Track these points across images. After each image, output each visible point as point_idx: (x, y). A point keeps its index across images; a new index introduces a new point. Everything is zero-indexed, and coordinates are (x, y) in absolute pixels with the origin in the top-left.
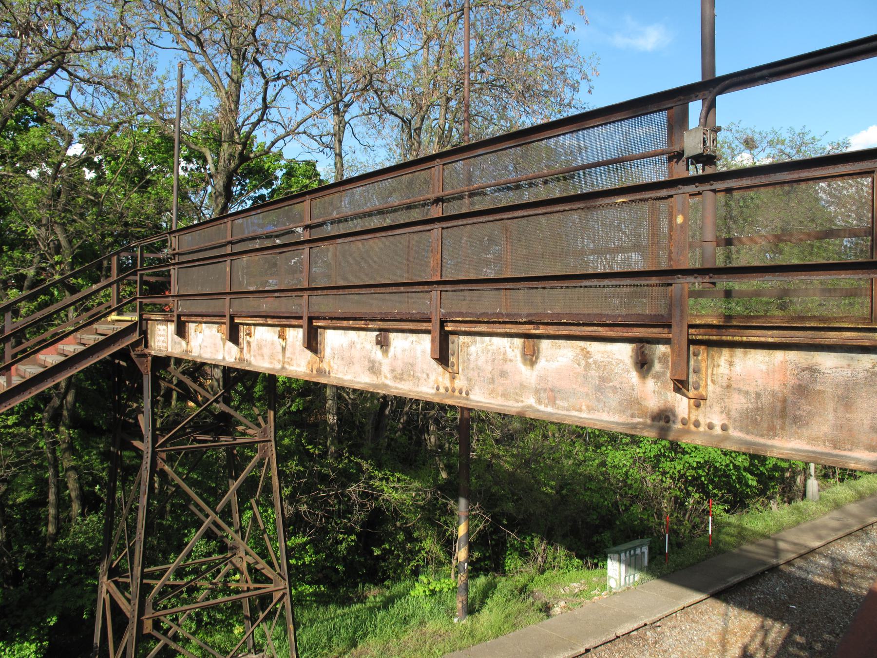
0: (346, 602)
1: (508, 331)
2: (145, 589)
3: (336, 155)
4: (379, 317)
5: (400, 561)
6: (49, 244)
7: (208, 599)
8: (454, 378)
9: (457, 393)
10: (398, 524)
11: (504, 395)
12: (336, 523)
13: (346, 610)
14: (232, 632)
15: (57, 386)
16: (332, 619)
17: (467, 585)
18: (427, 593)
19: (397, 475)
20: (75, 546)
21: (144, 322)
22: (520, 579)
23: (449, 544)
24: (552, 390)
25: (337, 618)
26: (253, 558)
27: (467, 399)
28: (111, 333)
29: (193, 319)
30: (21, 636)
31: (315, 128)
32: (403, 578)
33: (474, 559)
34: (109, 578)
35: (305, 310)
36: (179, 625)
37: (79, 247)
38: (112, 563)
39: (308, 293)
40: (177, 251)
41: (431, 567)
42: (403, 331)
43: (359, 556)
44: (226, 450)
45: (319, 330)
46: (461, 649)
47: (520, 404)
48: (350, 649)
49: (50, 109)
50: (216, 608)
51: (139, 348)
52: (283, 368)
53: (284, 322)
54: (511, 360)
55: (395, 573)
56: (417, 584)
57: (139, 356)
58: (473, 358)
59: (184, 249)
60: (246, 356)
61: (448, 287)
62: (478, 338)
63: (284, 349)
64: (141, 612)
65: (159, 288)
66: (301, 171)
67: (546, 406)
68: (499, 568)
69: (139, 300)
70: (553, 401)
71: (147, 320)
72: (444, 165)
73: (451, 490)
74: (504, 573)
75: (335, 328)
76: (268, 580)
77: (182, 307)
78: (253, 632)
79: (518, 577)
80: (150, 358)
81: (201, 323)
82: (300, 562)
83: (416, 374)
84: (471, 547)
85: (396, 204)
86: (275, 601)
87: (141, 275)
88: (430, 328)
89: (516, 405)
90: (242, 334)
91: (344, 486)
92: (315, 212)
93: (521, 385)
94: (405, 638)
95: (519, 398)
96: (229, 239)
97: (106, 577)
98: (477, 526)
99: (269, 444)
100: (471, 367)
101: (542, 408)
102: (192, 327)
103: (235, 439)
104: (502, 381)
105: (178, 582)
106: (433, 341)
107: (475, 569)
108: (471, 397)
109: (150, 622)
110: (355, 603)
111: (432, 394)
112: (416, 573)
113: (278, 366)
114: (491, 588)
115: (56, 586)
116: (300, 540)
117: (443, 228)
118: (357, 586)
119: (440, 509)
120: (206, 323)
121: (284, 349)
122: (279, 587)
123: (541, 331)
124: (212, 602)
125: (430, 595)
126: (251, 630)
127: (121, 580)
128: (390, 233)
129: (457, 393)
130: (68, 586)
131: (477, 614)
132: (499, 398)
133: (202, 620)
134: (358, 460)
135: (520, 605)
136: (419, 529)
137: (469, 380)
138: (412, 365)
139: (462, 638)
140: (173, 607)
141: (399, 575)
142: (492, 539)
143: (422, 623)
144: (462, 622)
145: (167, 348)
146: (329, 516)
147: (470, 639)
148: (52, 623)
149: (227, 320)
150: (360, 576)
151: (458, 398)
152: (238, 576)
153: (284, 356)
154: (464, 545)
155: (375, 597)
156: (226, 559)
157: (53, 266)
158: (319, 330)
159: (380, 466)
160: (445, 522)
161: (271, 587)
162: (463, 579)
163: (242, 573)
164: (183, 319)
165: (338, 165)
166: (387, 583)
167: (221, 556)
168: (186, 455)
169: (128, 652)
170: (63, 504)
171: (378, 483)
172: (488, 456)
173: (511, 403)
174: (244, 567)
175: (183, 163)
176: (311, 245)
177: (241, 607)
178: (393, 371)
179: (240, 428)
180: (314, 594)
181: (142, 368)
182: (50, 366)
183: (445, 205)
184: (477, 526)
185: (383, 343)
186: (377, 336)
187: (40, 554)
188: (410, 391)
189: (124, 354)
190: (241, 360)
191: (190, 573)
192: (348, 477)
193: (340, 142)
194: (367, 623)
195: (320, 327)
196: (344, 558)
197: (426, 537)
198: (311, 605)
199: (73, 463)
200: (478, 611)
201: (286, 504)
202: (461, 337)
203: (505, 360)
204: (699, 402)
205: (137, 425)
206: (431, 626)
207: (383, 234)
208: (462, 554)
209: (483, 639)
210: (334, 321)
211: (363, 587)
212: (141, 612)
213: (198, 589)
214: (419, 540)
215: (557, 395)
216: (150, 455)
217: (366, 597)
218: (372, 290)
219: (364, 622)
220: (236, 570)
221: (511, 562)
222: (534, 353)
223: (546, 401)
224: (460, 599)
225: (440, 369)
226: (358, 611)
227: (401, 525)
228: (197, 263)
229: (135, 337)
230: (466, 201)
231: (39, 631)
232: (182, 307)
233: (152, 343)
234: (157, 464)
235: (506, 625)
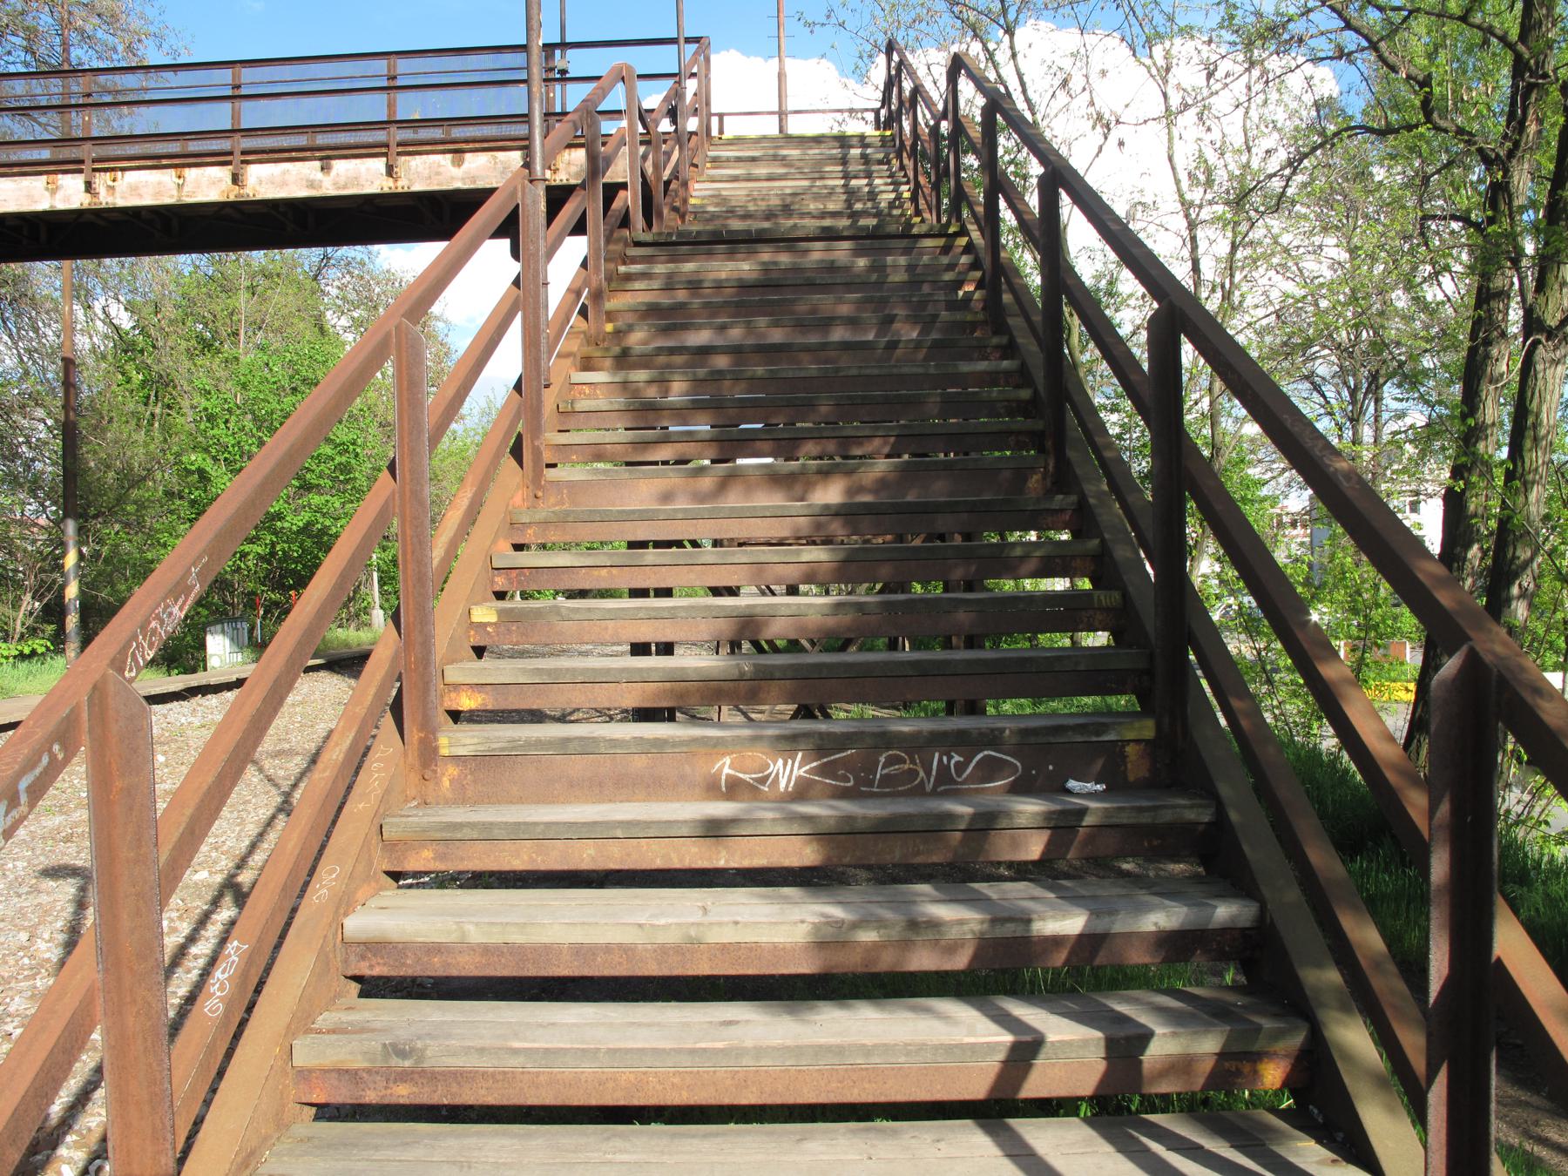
204: (555, 171)
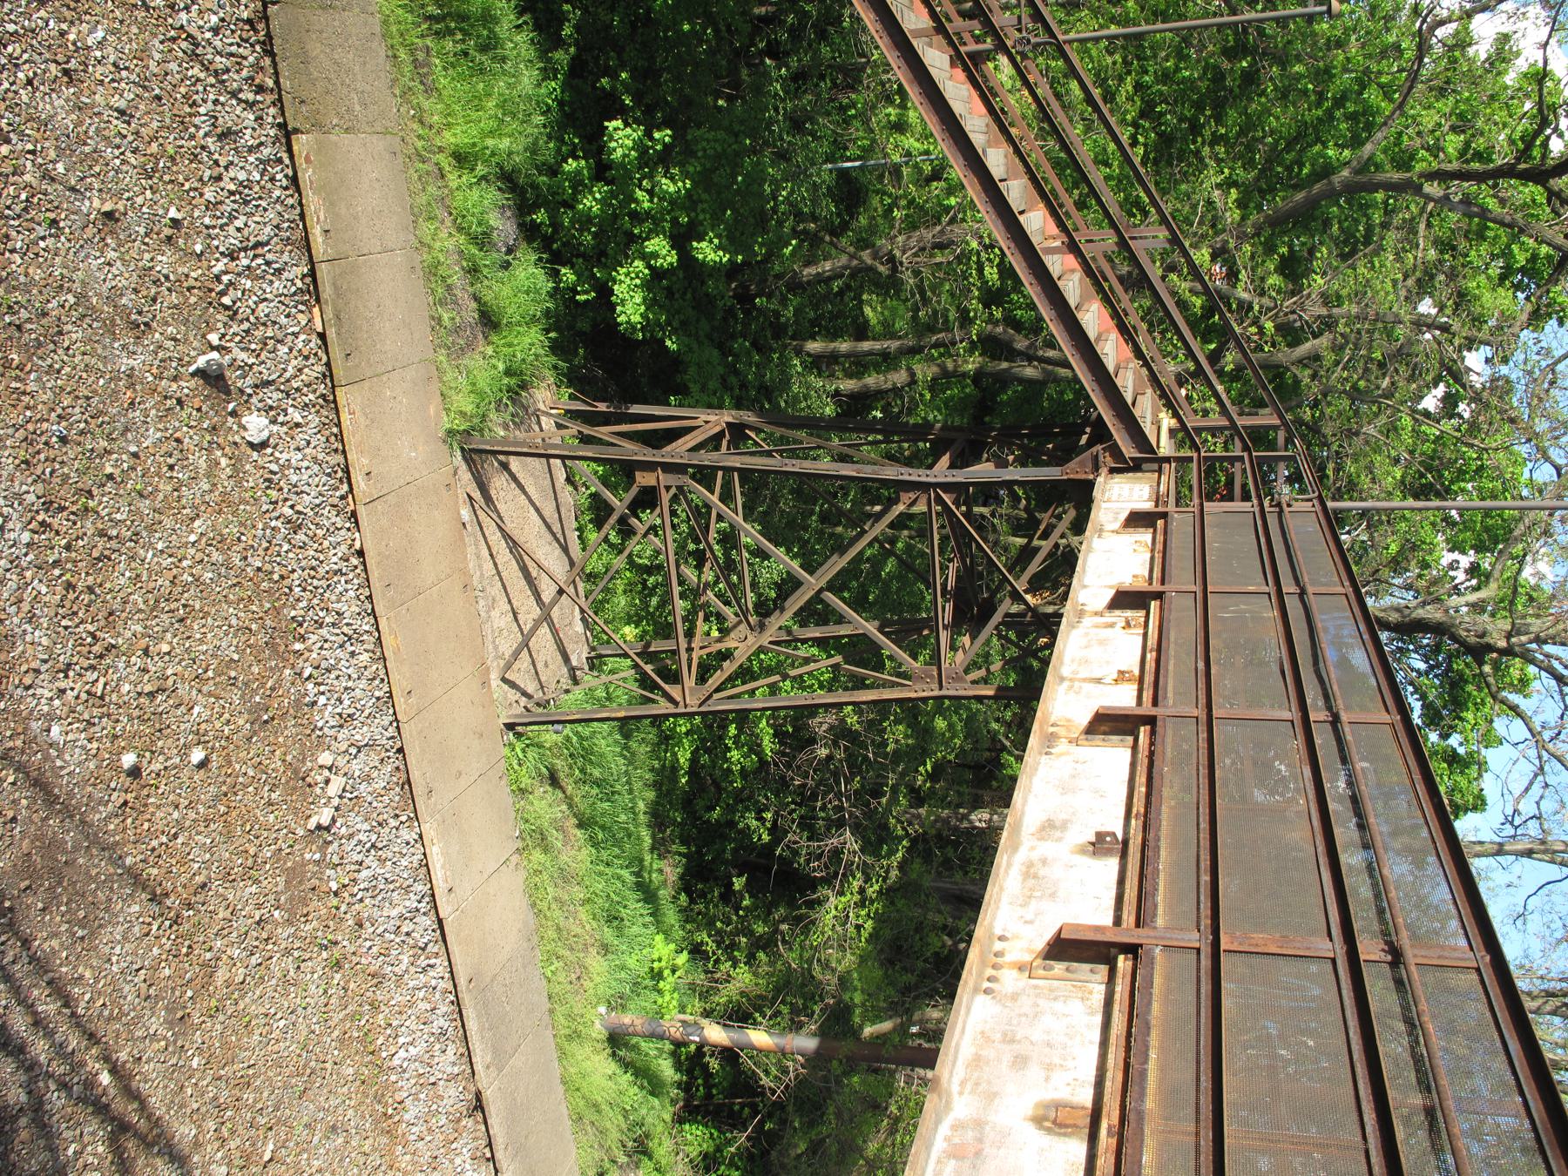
0: (658, 820)
1: (1109, 1075)
2: (705, 476)
3: (1501, 845)
4: (1151, 836)
5: (719, 924)
6: (1293, 312)
7: (681, 583)
8: (1020, 968)
9: (989, 972)
10: (784, 927)
11: (977, 1061)
12: (794, 811)
13: (642, 818)
14: (628, 624)
15: (1051, 344)
16: (631, 791)
17: (661, 1037)
18: (656, 965)
19: (869, 924)
20: (786, 383)
21: (1156, 466)
22: (663, 1148)
23: (739, 1015)
24: (978, 1154)
25: (631, 800)
26: (741, 657)
27: (976, 990)
28: (1137, 412)
29: (1160, 538)
30: (654, 299)
31: (1556, 806)
32: (688, 927)
33: (707, 1058)
34: (728, 424)
35: (1169, 712)
36: (645, 535)
37: (1297, 382)
38: (752, 428)
39: (1203, 717)
40: (1286, 509)
41: (700, 979)
42: (1121, 882)
43: (735, 851)
44: (929, 619)
45: (1130, 739)
46: (551, 1011)
47: (955, 1088)
48: (575, 815)
49: (1553, 322)
50: (666, 600)
51: (1108, 459)
52: (1062, 679)
53: (1149, 679)
54: (1047, 1079)
55: (699, 913)
56: (672, 946)
57: (1096, 458)
58: (1058, 1006)
59: (1291, 522)
60: (1088, 621)
61: (1206, 962)
62: (1098, 1019)
63: (1098, 681)
64: (669, 468)
65: (1216, 483)
66: (1463, 783)
67: (947, 1139)
68: (689, 1112)
69: (1195, 455)
70: (956, 1153)
71: (1160, 471)
72: (1478, 970)
73: (838, 1023)
74: (679, 1120)
75: (1133, 765)
76: (702, 679)
77: (1182, 521)
78: (626, 655)
79: (668, 1144)
80: (1091, 477)
81: (1152, 551)
82: (730, 743)
83: (1033, 902)
84: (729, 1055)
85: (1386, 872)
86: (666, 687)
87: (1241, 459)
88: (1124, 925)
89: (956, 1080)
90: (1129, 613)
91: (857, 829)
92: (1362, 730)
93: (995, 1094)
94: (583, 914)
95: (969, 1087)
96: (1310, 589)
97: (730, 420)
98: (767, 1073)
99: (935, 686)
100: (1041, 1002)
101: (944, 1130)
102: (1146, 536)
103: (946, 628)
104: (1007, 1058)
105: (713, 535)
106: (1098, 929)
107: (692, 1061)
108: (981, 999)
109: (653, 483)
110: (653, 837)
111: (991, 926)
112: (697, 951)
113: (1066, 671)
114: (654, 1086)
115: (725, 351)
116: (768, 745)
117: (1334, 961)
118: (683, 843)
119: (805, 1007)
120: (1152, 558)
121: (1098, 681)
122: (689, 695)
123: (1105, 1140)
124: (676, 589)
125: (652, 969)
126: (631, 653)
127: (725, 443)
128: (1323, 860)
129: (989, 972)
130: (721, 370)
131: (609, 1051)
132: (973, 1050)
133: (650, 574)
134: (900, 854)
135: (614, 1135)
136: (771, 963)
137: (1014, 997)
138: (1053, 895)
139: (569, 1016)
140: (674, 527)
141: (694, 921)
142: (743, 1106)
143: (605, 949)
144: (597, 1022)
145: (1109, 501)
146: (806, 798)
147: (567, 1031)
148: (668, 343)
149: (1156, 587)
150: (699, 852)
151: (980, 974)
152: (715, 634)
153: (1084, 680)
154: (731, 1040)
155: (660, 871)
156: (745, 613)
157: (1255, 322)
158: (1130, 739)
159: (887, 894)
160: (777, 1014)
161: (690, 681)
162: (673, 1030)
163: (719, 640)
164: (1160, 523)
165: (1478, 848)
166: (683, 897)
167: (750, 606)
168: (922, 554)
169: (611, 449)
170: (859, 364)
171: (856, 884)
172: (893, 1109)
173: (960, 1072)
174: (730, 643)
175: (1465, 561)
176: (1298, 723)
177: (667, 637)
178: (1044, 862)
179: (966, 639)
180: (675, 768)
181: (1072, 464)
182: (1079, 316)
183: (1386, 968)
184: (767, 1073)
185: (1100, 845)
186: (1114, 834)
187: (779, 330)
188: (1001, 889)
189: (1101, 434)
190: (1081, 614)
191: (727, 555)
192: (876, 837)
193: (1529, 853)
194: (617, 851)
195: (1136, 740)
196: (732, 824)
197: (755, 974)
198: (658, 758)
199: (920, 376)
200: (614, 1054)
201: (831, 719)
202: (1103, 987)
203: (1049, 1067)
205: (975, 459)
206: (597, 964)
207: (1321, 849)
208: (716, 1034)
209: (563, 1054)
210: (1146, 761)
211: (680, 854)
212: (669, 468)
213: (699, 567)
214: (751, 959)
215: (967, 1163)
216: (923, 479)
217: (661, 857)
218: (1204, 825)
219: (618, 843)
220: (725, 632)
221: (697, 1137)
222: (1061, 1126)
223: (957, 1140)
224: (638, 1022)
225: (1041, 942)
226: (639, 838)
227: (782, 933)
228: (1263, 540)
229: (1129, 451)
230: (1417, 1100)
231: (659, 325)
232: (1182, 521)
233: (1118, 478)
234: (907, 491)
235: (582, 1103)
